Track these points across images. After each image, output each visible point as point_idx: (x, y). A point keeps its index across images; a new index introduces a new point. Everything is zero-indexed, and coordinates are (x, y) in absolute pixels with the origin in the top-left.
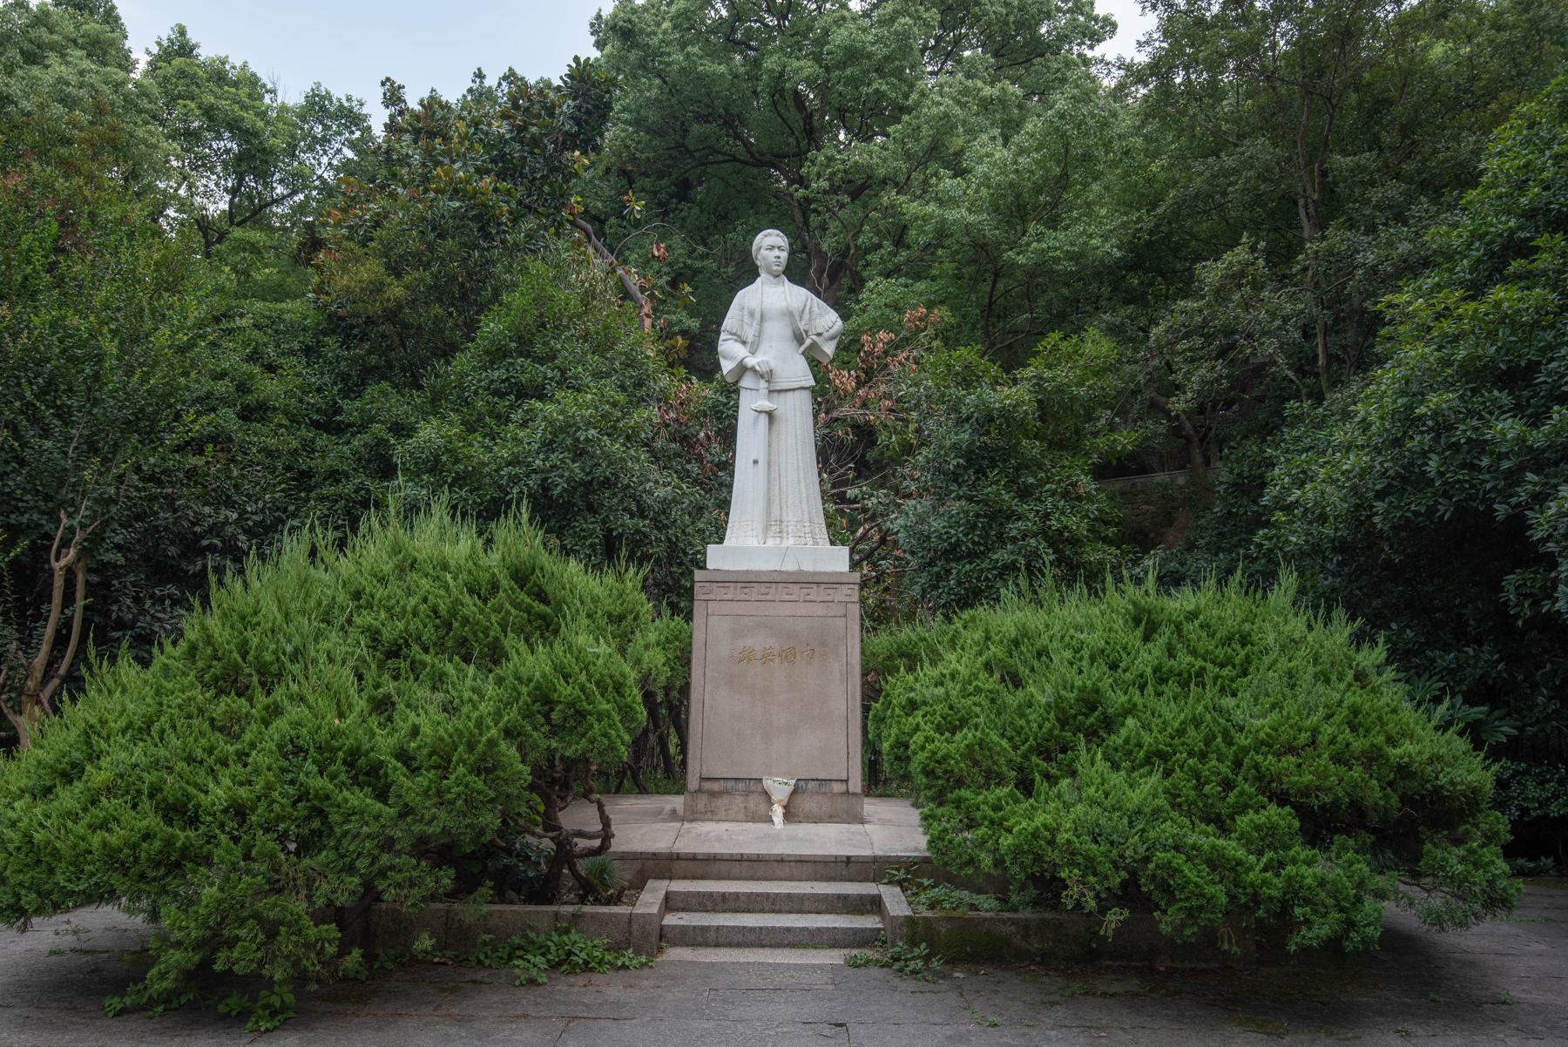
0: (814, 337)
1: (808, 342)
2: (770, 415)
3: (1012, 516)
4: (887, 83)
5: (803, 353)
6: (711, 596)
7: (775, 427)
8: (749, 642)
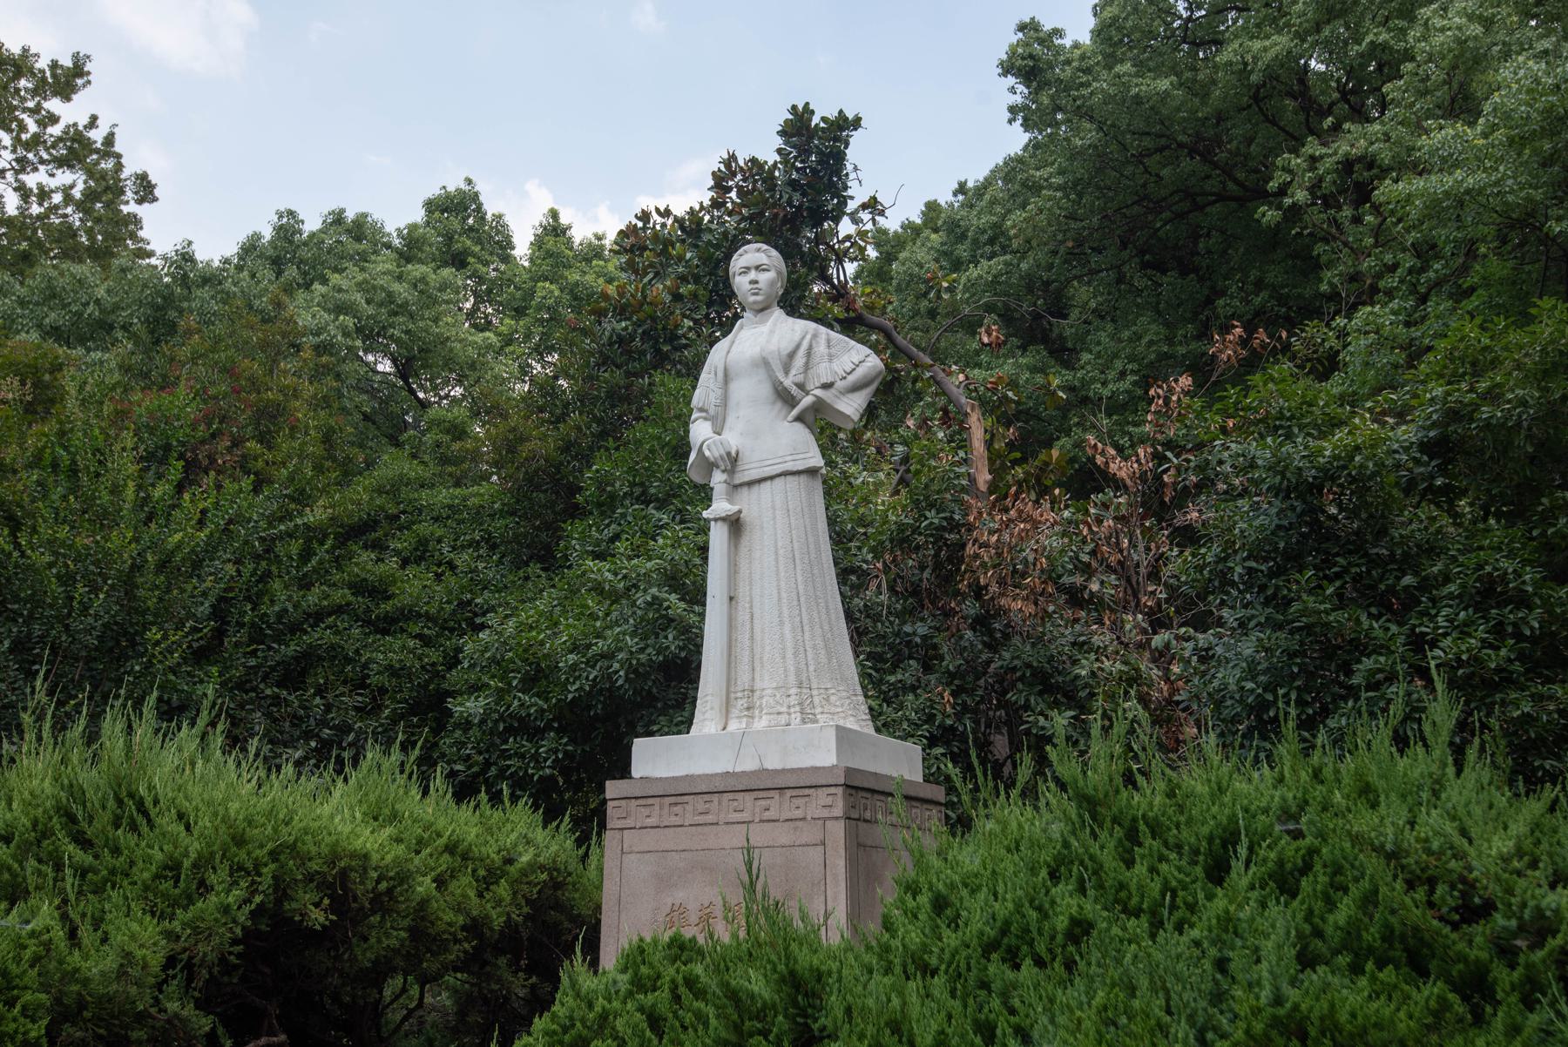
0: (819, 392)
3: (1360, 647)
4: (1389, 30)
6: (629, 823)
7: (745, 541)
8: (680, 896)
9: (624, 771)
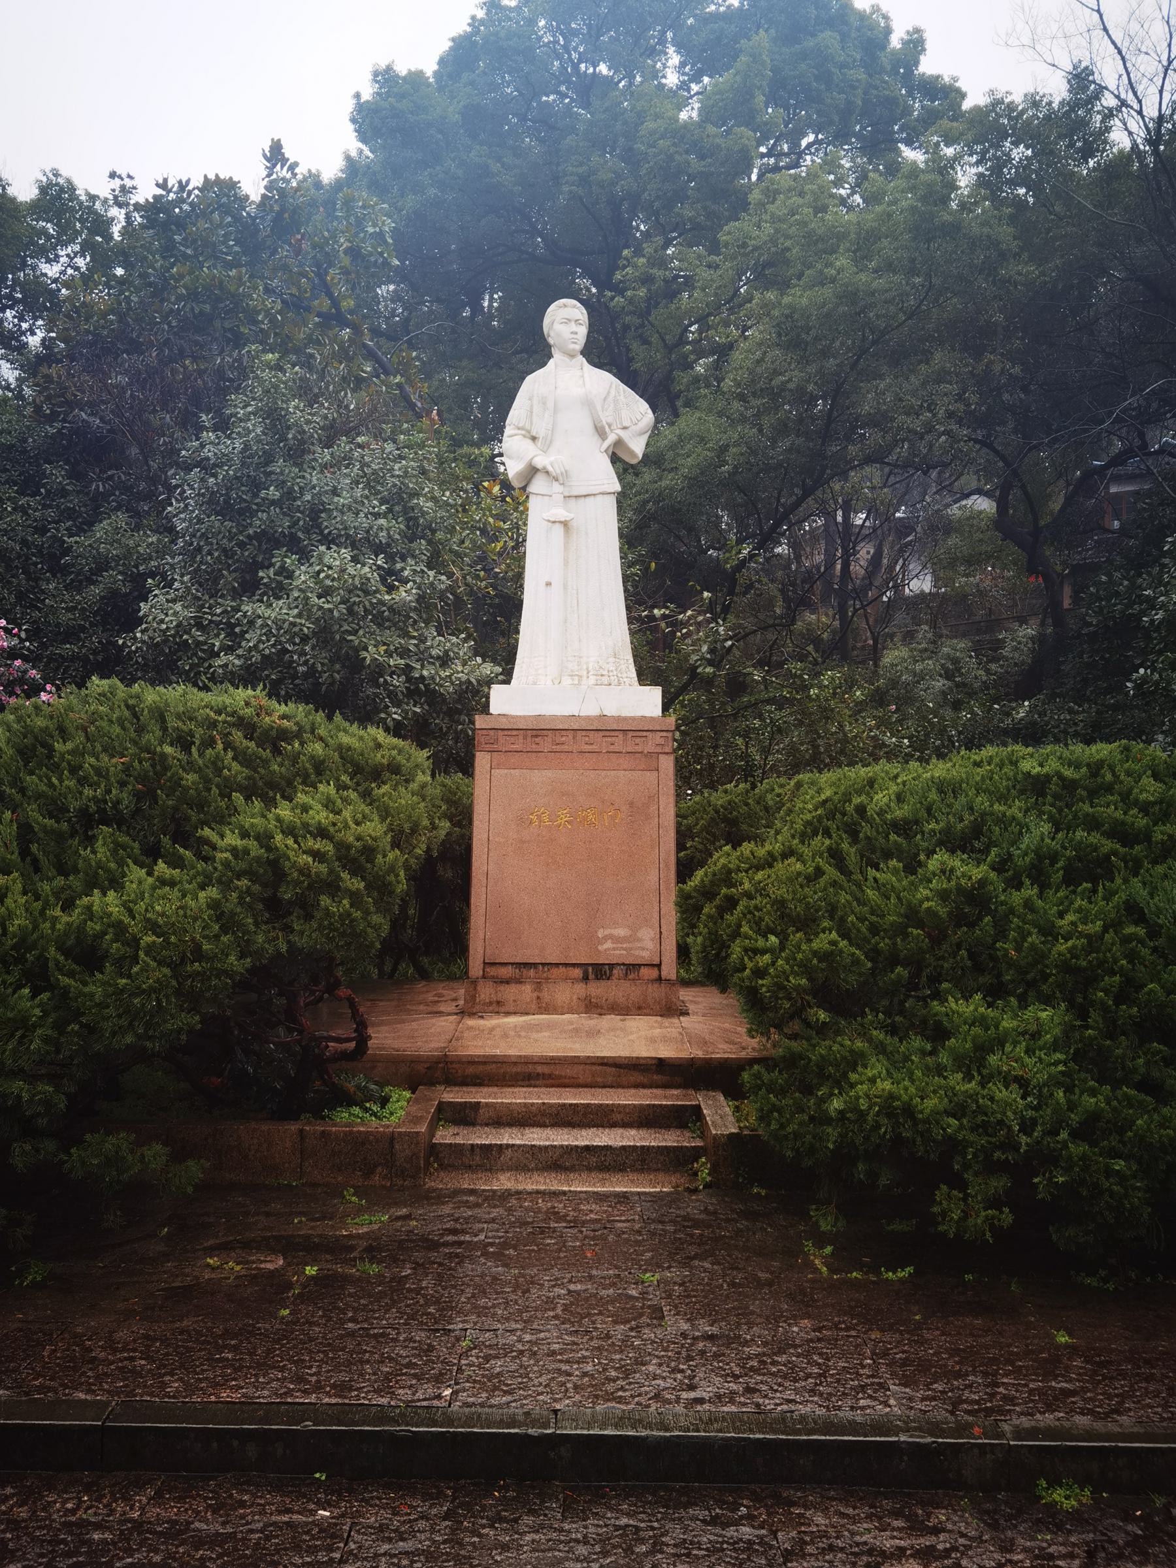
1: (611, 438)
2: (565, 524)
5: (606, 451)
9: (485, 709)
